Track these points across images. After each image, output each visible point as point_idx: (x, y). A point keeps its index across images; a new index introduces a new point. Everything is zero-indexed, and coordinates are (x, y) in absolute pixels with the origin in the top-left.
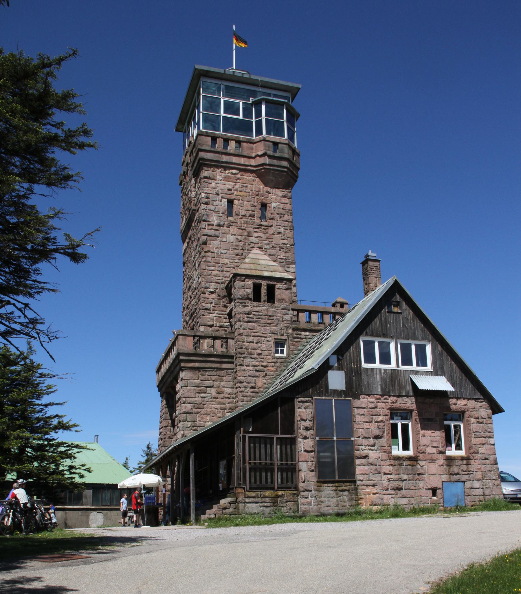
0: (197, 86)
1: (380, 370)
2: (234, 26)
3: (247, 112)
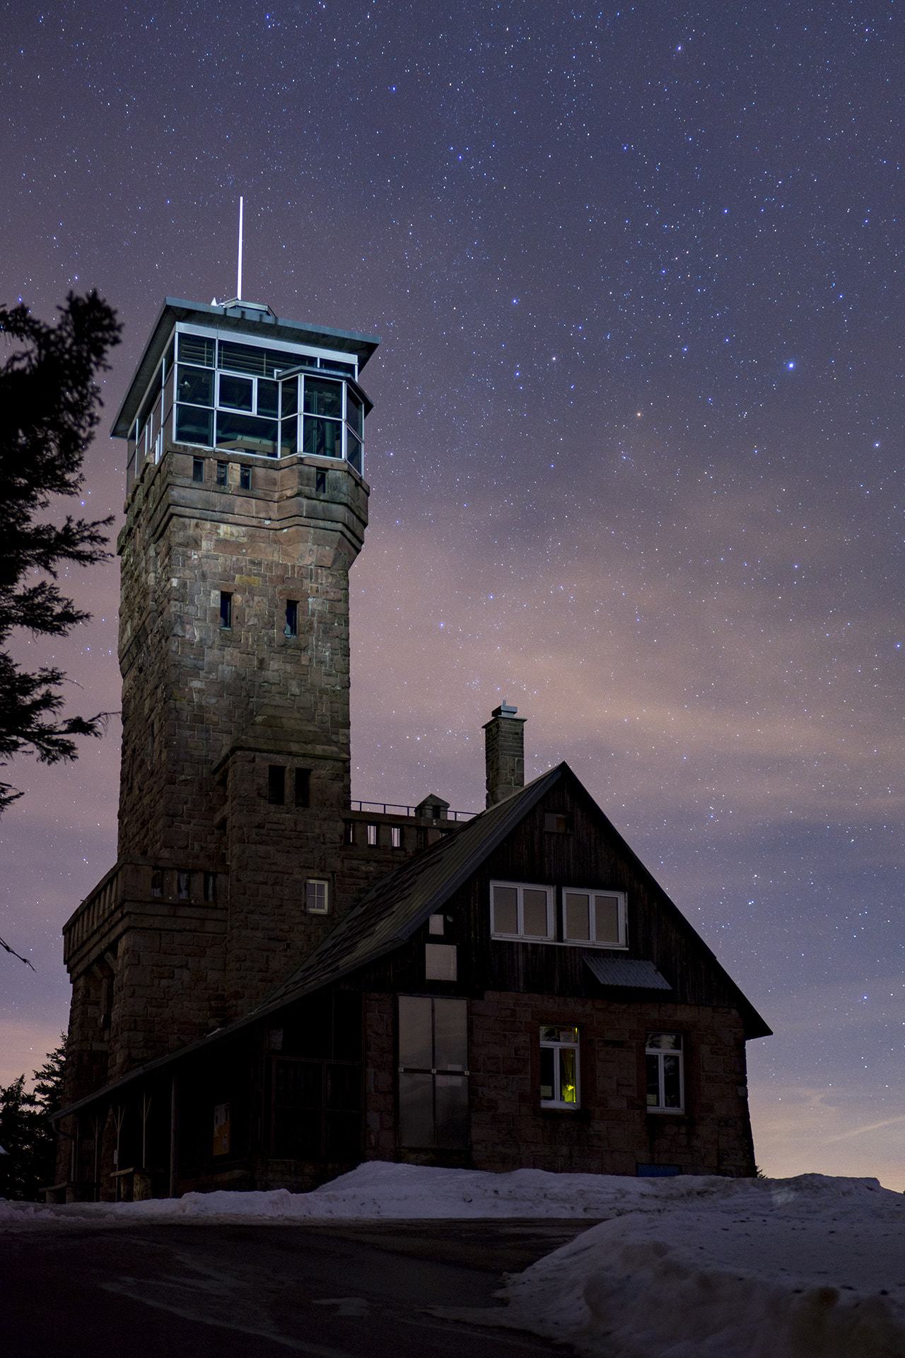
0: (169, 335)
1: (525, 945)
2: (241, 198)
3: (267, 401)
